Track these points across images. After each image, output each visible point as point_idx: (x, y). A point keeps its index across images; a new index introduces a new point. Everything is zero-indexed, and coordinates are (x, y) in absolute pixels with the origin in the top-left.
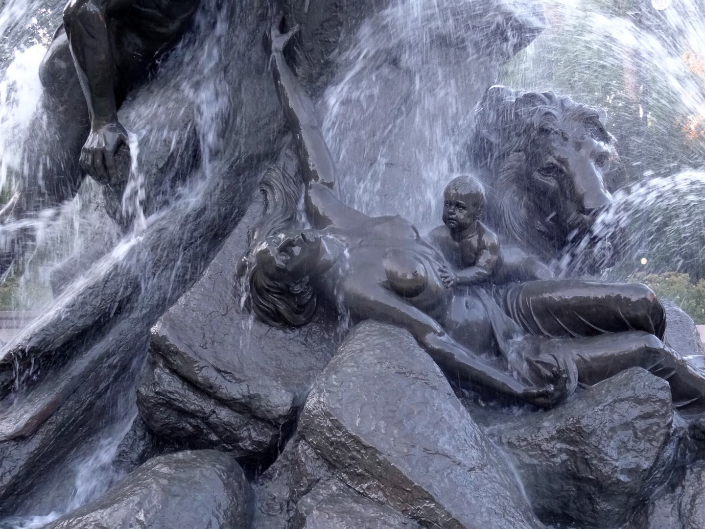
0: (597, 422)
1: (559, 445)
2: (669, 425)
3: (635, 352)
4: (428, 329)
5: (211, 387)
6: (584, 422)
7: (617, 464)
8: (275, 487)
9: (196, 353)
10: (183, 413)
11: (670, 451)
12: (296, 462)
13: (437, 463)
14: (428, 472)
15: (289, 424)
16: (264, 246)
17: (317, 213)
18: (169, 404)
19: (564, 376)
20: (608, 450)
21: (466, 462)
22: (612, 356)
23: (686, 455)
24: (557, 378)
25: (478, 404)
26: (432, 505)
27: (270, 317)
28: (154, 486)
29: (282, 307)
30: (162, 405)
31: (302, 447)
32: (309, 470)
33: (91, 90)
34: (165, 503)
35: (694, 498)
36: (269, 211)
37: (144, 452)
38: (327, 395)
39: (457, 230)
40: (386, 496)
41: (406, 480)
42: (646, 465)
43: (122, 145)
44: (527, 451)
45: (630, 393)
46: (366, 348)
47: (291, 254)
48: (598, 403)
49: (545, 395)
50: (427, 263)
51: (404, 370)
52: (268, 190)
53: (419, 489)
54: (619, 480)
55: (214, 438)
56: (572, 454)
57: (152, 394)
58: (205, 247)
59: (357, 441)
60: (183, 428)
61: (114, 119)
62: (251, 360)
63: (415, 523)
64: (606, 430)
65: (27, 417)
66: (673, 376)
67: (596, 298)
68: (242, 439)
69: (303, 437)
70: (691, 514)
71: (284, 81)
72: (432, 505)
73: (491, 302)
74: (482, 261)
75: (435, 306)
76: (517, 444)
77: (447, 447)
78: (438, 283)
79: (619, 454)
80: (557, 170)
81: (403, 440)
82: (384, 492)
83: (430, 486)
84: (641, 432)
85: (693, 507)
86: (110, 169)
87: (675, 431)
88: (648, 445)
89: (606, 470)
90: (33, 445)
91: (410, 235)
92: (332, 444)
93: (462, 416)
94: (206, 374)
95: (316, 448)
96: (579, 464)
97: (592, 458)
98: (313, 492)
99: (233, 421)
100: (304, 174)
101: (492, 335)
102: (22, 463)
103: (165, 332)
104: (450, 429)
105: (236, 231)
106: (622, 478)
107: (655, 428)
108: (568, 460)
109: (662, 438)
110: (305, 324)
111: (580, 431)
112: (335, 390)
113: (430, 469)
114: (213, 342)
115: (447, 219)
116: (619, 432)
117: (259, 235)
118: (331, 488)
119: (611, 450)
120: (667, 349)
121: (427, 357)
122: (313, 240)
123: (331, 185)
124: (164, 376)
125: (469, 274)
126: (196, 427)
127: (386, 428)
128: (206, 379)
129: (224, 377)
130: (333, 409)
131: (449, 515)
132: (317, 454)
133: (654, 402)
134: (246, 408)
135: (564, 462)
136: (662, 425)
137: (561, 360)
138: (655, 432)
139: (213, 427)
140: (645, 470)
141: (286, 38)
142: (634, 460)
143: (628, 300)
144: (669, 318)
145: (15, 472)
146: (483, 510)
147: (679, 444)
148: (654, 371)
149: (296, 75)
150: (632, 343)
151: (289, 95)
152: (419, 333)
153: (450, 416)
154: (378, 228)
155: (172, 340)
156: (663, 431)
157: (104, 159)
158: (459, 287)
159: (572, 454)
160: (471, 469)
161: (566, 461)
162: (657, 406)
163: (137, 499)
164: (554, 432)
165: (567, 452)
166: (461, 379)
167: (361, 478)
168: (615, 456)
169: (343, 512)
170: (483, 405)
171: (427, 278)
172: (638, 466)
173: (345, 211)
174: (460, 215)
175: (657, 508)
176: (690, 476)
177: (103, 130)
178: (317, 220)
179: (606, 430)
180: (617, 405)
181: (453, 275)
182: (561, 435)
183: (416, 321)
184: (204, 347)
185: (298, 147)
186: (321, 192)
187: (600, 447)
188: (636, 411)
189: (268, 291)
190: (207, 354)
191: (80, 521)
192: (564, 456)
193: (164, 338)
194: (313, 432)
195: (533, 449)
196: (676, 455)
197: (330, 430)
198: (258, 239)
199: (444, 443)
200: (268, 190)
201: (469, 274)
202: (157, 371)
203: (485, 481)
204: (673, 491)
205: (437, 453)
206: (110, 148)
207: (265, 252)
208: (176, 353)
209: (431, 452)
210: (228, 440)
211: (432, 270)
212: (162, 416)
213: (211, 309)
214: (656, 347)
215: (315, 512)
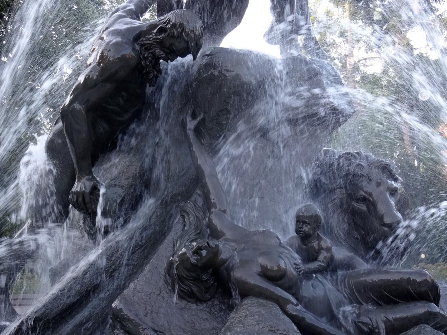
4: (289, 302)
9: (140, 319)
16: (184, 250)
19: (377, 331)
22: (407, 317)
27: (187, 295)
29: (195, 289)
36: (186, 228)
43: (95, 189)
47: (201, 255)
51: (274, 329)
52: (186, 215)
61: (91, 173)
71: (194, 148)
73: (329, 285)
74: (321, 257)
75: (292, 288)
91: (274, 241)
103: (121, 306)
105: (166, 241)
110: (210, 300)
114: (152, 312)
121: (288, 320)
122: (214, 246)
123: (224, 212)
125: (313, 266)
137: (374, 320)
141: (196, 122)
149: (202, 144)
150: (420, 309)
151: (198, 156)
152: (282, 304)
155: (125, 312)
174: (306, 228)
177: (84, 180)
190: (148, 320)
193: (121, 310)
198: (178, 246)
201: (313, 266)
202: (116, 331)
207: (184, 254)
208: (128, 319)
211: (290, 261)
213: (151, 291)
214: (435, 311)
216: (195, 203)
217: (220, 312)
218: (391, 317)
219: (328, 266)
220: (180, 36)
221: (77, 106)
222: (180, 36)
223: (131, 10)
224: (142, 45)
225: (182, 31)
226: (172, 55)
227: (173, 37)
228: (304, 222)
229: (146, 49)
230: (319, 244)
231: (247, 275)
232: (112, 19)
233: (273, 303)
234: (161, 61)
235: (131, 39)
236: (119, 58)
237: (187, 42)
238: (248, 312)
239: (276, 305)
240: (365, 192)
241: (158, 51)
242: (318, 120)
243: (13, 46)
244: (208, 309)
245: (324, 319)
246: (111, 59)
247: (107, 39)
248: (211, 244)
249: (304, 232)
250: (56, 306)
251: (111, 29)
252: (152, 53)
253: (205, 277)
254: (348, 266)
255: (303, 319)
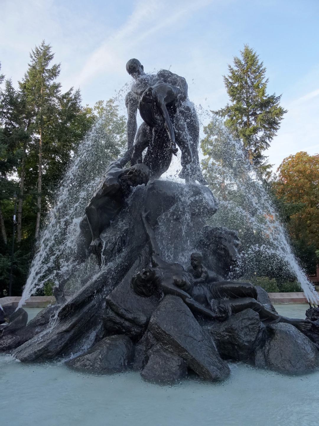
0: (237, 326)
1: (226, 333)
2: (260, 327)
3: (248, 304)
4: (187, 297)
5: (123, 315)
6: (233, 326)
7: (244, 339)
8: (141, 347)
9: (119, 305)
10: (115, 323)
11: (260, 335)
12: (147, 339)
13: (189, 339)
14: (186, 342)
15: (146, 325)
16: (139, 272)
17: (155, 262)
18: (111, 320)
19: (227, 311)
20: (241, 335)
21: (197, 339)
22: (241, 305)
23: (265, 336)
24: (225, 312)
25: (202, 320)
26: (187, 353)
27: (141, 294)
28: (105, 347)
29: (144, 291)
30: (109, 320)
31: (149, 334)
32: (151, 341)
33: (93, 230)
34: (107, 352)
35: (268, 350)
36: (141, 262)
37: (104, 335)
38: (156, 317)
39: (195, 267)
40: (173, 350)
41: (179, 345)
42: (253, 340)
43: (100, 245)
44: (216, 335)
45: (247, 317)
46: (168, 303)
47: (147, 275)
48: (237, 320)
49: (222, 317)
50: (186, 277)
51: (179, 310)
52: (141, 256)
53: (183, 348)
54: (245, 345)
55: (124, 331)
56: (230, 336)
57: (106, 317)
58: (123, 273)
59: (164, 332)
60: (115, 328)
61: (99, 237)
62: (135, 307)
63: (182, 359)
64: (240, 328)
65: (70, 324)
66: (260, 311)
67: (236, 287)
68: (132, 331)
69: (149, 331)
70: (268, 356)
71: (146, 226)
72: (187, 353)
73: (206, 289)
74: (202, 276)
75: (189, 290)
76: (213, 333)
77: (192, 334)
78: (190, 283)
79: (245, 336)
80: (225, 250)
81: (178, 332)
82: (173, 349)
83: (186, 347)
84: (251, 329)
85: (268, 353)
86: (97, 250)
87: (262, 329)
88: (253, 333)
89: (241, 341)
90: (71, 333)
91: (181, 269)
92: (157, 333)
93: (196, 324)
94: (122, 311)
95: (153, 334)
96: (232, 339)
97: (236, 338)
98: (152, 348)
99: (129, 325)
100: (151, 252)
101: (206, 298)
102: (67, 339)
103: (110, 299)
104: (193, 328)
105: (132, 268)
106: (246, 344)
107: (255, 328)
108: (229, 338)
109: (258, 331)
110: (151, 296)
111: (232, 329)
112: (159, 316)
113: (187, 341)
114: (124, 301)
115: (192, 264)
116: (244, 329)
117: (138, 269)
118: (157, 347)
119: (242, 334)
120: (258, 302)
121: (186, 305)
122: (153, 271)
123: (158, 255)
124: (110, 312)
125: (199, 280)
126: (119, 327)
127: (173, 328)
128: (122, 312)
129: (127, 312)
130: (158, 322)
131: (192, 357)
132: (153, 336)
133: (255, 320)
134: (133, 321)
135: (228, 339)
136: (257, 327)
137: (226, 306)
138: (255, 329)
139: (124, 327)
140: (253, 341)
141: (146, 214)
142: (249, 338)
143: (245, 287)
144: (258, 292)
145: (65, 342)
146: (203, 355)
147: (263, 333)
148: (254, 310)
149: (149, 224)
150: (247, 301)
151: (147, 229)
152: (183, 298)
153: (193, 324)
154: (172, 267)
155: (112, 301)
156: (258, 329)
157: (95, 248)
158: (196, 284)
159: (230, 336)
160: (199, 341)
161: (228, 338)
162: (255, 321)
163: (99, 351)
164: (225, 329)
165: (229, 335)
166: (196, 312)
167: (165, 344)
168: (243, 337)
169: (160, 355)
170: (204, 320)
171: (186, 281)
172: (251, 340)
173: (164, 262)
174: (195, 263)
175: (257, 354)
176: (267, 343)
177: (96, 240)
178: (155, 265)
179: (240, 328)
180: (243, 320)
181: (194, 280)
182: (227, 330)
183: (183, 294)
184: (121, 303)
185: (150, 244)
186: (156, 256)
187: (239, 334)
188: (249, 323)
189: (140, 286)
190: (122, 305)
191: (82, 358)
192: (228, 337)
193: (110, 300)
194: (152, 329)
195: (218, 335)
196: (262, 336)
197: (157, 329)
198: (135, 272)
199: (191, 333)
200: (141, 256)
201: (199, 280)
202: (108, 310)
203: (204, 345)
204: (262, 348)
205: (189, 336)
206: (97, 245)
207: (139, 274)
208: (113, 305)
209: (187, 336)
210: (128, 331)
211: (187, 279)
212: (109, 324)
213: (124, 291)
214: (254, 302)
215: (152, 355)
216: (145, 250)
217: (156, 301)
218: (234, 304)
219: (206, 280)
220: (139, 176)
221: (93, 207)
222: (139, 176)
223: (118, 164)
224: (122, 180)
225: (140, 173)
226: (135, 184)
227: (136, 176)
228: (195, 260)
229: (124, 181)
230: (201, 270)
231: (168, 284)
232: (110, 168)
233: (179, 297)
234: (131, 186)
235: (117, 177)
236: (111, 186)
237: (142, 178)
238: (167, 302)
239: (181, 299)
240: (224, 246)
241: (129, 182)
242: (202, 211)
243: (33, 307)
244: (150, 300)
245: (204, 305)
246: (108, 186)
247: (107, 177)
248: (151, 270)
249: (195, 264)
250: (81, 298)
251: (108, 173)
252: (126, 183)
253: (149, 285)
254: (214, 280)
255: (193, 305)
